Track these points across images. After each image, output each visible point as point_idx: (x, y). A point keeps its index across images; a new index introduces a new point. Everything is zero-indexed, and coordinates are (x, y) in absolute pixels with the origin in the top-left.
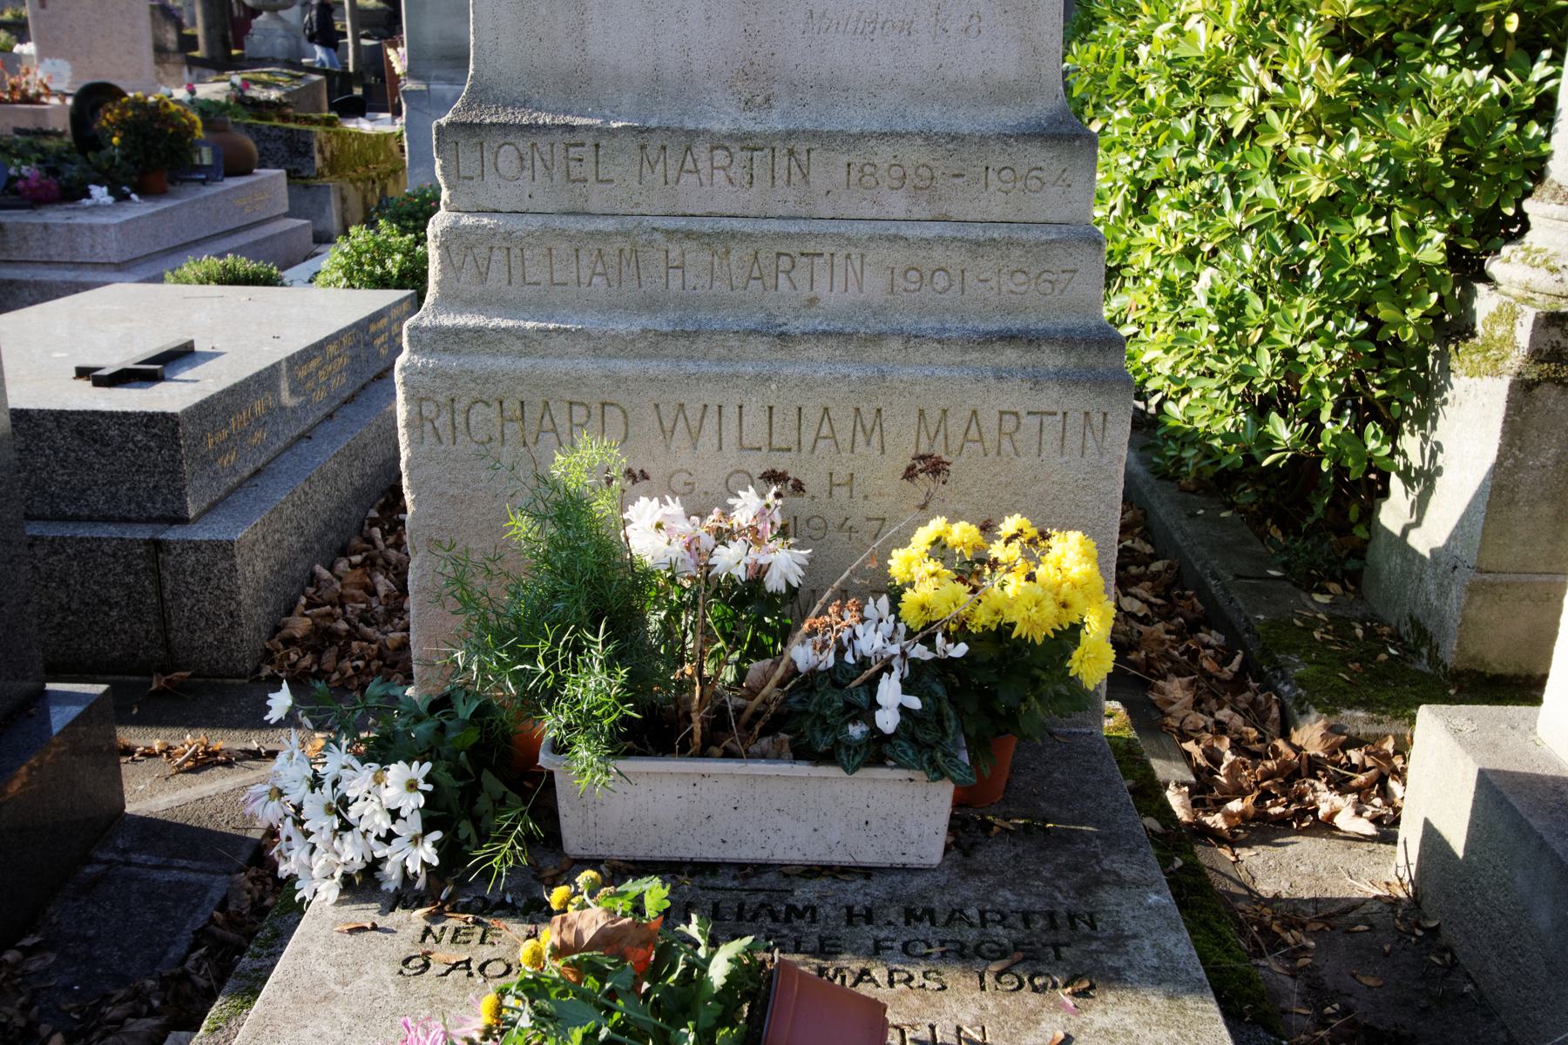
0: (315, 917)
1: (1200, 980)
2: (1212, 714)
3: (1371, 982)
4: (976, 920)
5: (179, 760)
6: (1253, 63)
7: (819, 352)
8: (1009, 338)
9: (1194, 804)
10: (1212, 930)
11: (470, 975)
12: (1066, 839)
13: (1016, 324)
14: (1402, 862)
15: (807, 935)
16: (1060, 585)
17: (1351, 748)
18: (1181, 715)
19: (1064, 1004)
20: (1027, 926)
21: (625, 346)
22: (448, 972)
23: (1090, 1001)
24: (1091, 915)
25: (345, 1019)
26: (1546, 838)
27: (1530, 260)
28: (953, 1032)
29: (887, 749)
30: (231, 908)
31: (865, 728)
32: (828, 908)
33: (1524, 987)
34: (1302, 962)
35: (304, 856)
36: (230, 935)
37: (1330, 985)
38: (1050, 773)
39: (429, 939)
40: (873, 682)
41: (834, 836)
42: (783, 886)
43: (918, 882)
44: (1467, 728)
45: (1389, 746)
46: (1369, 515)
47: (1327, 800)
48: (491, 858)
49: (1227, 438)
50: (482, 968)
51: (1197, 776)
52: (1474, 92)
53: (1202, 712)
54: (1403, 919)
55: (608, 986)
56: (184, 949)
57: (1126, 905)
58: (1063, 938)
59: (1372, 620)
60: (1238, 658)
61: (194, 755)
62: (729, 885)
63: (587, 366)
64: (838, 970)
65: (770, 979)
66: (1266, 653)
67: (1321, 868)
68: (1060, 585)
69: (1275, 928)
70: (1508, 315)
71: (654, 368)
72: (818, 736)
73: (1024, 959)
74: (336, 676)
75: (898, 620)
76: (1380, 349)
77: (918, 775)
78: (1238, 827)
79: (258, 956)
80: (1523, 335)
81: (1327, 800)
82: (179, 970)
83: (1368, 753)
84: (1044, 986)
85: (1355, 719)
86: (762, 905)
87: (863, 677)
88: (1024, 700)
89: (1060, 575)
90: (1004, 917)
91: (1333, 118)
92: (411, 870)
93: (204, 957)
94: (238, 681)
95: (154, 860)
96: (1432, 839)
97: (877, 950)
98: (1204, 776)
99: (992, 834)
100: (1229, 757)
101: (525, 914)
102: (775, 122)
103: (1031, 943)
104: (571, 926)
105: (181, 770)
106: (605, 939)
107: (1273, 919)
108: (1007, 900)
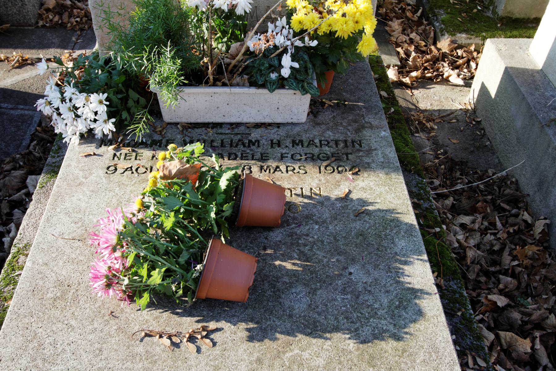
0: (71, 150)
1: (398, 167)
2: (408, 35)
3: (455, 141)
4: (318, 144)
5: (13, 63)
9: (399, 73)
10: (403, 137)
11: (133, 173)
12: (352, 109)
14: (472, 98)
15: (256, 152)
16: (355, 13)
17: (459, 49)
18: (397, 36)
19: (349, 178)
20: (337, 147)
22: (124, 172)
23: (358, 176)
24: (360, 141)
25: (88, 193)
26: (525, 95)
28: (309, 190)
29: (285, 82)
30: (43, 125)
31: (277, 75)
32: (264, 141)
33: (508, 145)
34: (432, 134)
35: (63, 127)
36: (45, 136)
37: (441, 143)
38: (348, 80)
39: (116, 158)
41: (266, 113)
42: (247, 132)
43: (297, 129)
44: (503, 49)
45: (472, 48)
47: (446, 70)
48: (135, 130)
50: (137, 170)
51: (401, 62)
53: (405, 34)
54: (469, 118)
55: (182, 190)
56: (28, 141)
57: (373, 136)
58: (349, 151)
60: (420, 11)
61: (18, 61)
62: (227, 132)
64: (268, 167)
65: (243, 183)
66: (431, 9)
67: (442, 97)
68: (355, 13)
69: (424, 122)
72: (259, 77)
73: (336, 160)
74: (69, 25)
75: (290, 28)
77: (298, 92)
78: (414, 81)
79: (54, 157)
81: (446, 70)
82: (27, 151)
83: (464, 51)
84: (342, 171)
85: (462, 38)
86: (239, 140)
87: (276, 53)
88: (339, 60)
90: (328, 143)
92: (105, 133)
93: (37, 145)
94: (30, 28)
95: (10, 106)
96: (484, 89)
97: (282, 158)
98: (403, 61)
99: (325, 107)
100: (413, 54)
101: (151, 147)
103: (338, 154)
104: (167, 168)
105: (14, 68)
106: (180, 174)
107: (424, 118)
108: (330, 136)
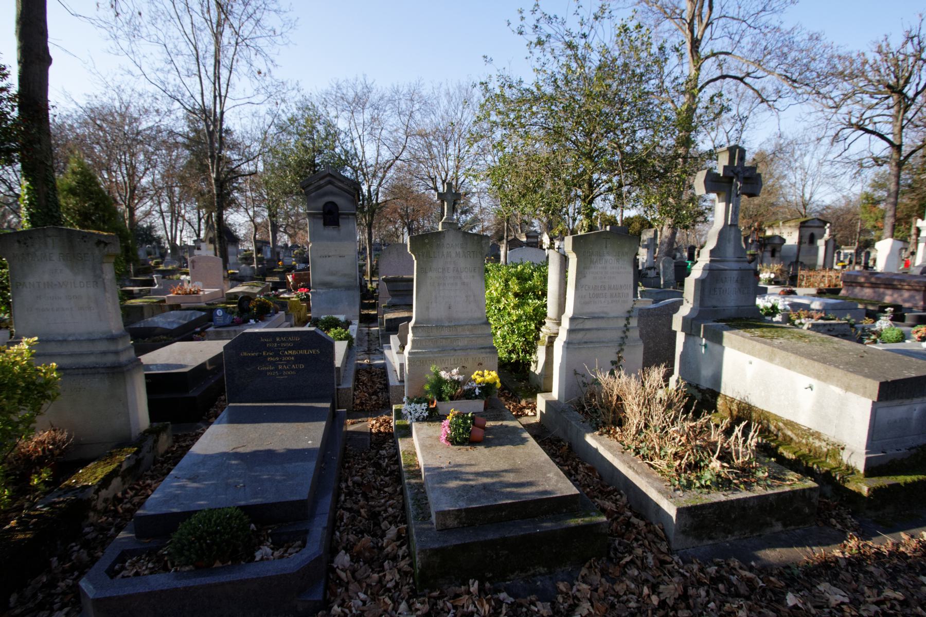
21: (436, 353)
46: (529, 369)
47: (527, 411)
70: (544, 337)
76: (527, 342)
89: (491, 376)
91: (516, 307)
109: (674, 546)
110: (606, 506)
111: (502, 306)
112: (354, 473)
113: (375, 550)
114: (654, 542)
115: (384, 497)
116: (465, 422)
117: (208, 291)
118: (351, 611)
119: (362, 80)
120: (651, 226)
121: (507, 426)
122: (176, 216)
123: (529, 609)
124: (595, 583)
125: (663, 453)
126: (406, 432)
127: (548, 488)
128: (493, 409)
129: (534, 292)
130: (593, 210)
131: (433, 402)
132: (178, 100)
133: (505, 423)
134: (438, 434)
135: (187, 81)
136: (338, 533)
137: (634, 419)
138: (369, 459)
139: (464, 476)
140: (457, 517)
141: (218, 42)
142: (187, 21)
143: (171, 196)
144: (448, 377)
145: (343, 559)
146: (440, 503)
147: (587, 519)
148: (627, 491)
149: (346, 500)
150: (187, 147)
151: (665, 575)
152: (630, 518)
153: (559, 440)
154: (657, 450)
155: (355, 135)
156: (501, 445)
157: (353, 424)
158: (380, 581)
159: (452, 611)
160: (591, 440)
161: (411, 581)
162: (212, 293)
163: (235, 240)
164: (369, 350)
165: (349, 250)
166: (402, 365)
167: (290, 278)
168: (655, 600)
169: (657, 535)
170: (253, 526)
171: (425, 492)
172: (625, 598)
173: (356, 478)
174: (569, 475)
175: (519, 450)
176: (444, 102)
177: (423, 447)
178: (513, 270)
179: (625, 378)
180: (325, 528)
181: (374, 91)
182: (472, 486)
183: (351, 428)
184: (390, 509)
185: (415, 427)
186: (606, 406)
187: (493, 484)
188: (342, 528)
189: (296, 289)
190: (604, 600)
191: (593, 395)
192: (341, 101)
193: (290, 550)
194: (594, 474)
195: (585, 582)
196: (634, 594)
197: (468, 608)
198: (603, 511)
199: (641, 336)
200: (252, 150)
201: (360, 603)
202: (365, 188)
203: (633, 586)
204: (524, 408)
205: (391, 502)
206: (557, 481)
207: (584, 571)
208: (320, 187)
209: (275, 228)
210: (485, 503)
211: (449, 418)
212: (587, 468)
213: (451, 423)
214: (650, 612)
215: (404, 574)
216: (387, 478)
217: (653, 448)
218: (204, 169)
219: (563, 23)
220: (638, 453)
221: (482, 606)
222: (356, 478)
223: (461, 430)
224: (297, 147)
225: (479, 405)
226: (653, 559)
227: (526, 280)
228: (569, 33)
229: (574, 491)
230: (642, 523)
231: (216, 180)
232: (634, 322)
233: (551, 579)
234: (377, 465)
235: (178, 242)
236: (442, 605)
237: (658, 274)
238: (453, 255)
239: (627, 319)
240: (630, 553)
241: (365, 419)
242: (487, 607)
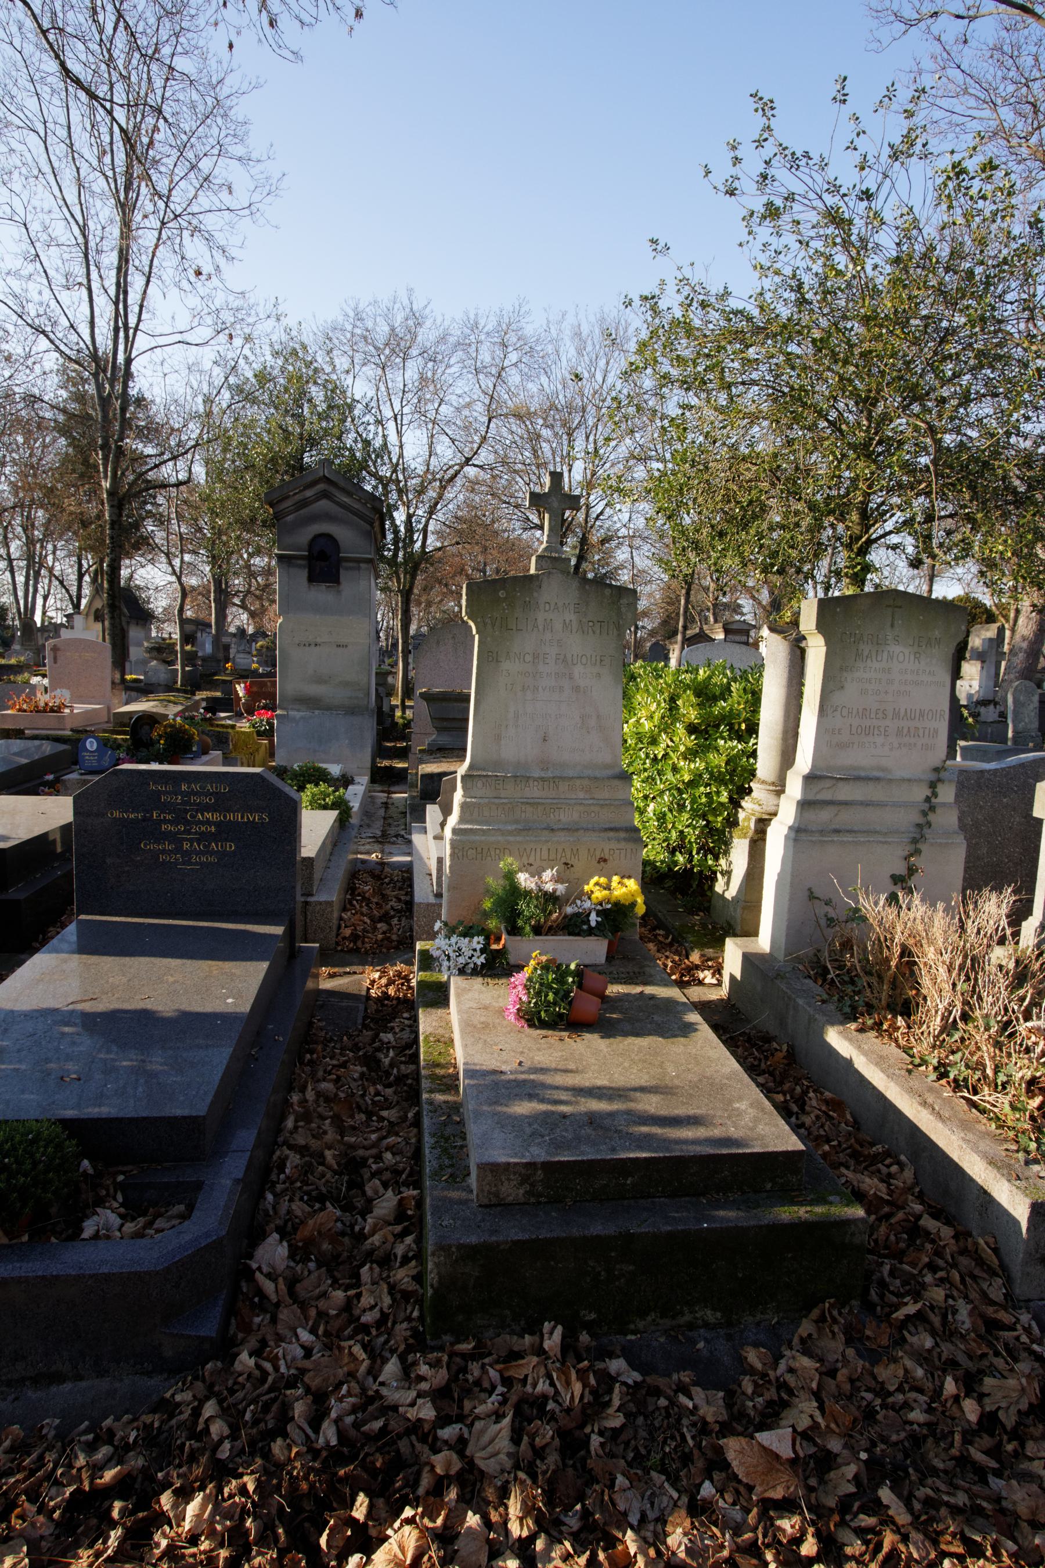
6: (664, 736)
7: (562, 834)
8: (611, 829)
13: (612, 825)
21: (510, 833)
27: (754, 801)
40: (589, 915)
46: (712, 887)
49: (662, 862)
52: (733, 748)
59: (714, 924)
63: (500, 838)
71: (518, 839)
76: (710, 830)
80: (752, 825)
89: (627, 888)
91: (691, 754)
96: (732, 977)
102: (550, 774)
109: (1020, 1290)
110: (864, 1187)
111: (660, 753)
112: (320, 1073)
113: (346, 1240)
114: (974, 1278)
115: (378, 1129)
116: (561, 980)
117: (79, 708)
118: (276, 1368)
119: (406, 302)
120: (991, 618)
121: (652, 997)
122: (35, 566)
123: (673, 1403)
124: (831, 1357)
125: (1002, 1078)
126: (437, 996)
127: (733, 1132)
128: (625, 961)
129: (731, 726)
130: (867, 568)
131: (498, 939)
132: (43, 332)
133: (649, 990)
134: (501, 1003)
135: (64, 296)
136: (270, 1197)
137: (938, 990)
138: (356, 1048)
139: (549, 1094)
140: (524, 1180)
141: (126, 224)
142: (67, 175)
143: (28, 526)
144: (533, 886)
145: (274, 1252)
146: (490, 1146)
147: (819, 1210)
148: (914, 1158)
149: (296, 1128)
150: (63, 430)
151: (997, 1354)
152: (919, 1217)
153: (768, 1039)
154: (989, 1072)
155: (388, 413)
156: (637, 1034)
157: (332, 976)
158: (348, 1306)
159: (500, 1389)
160: (838, 1040)
161: (416, 1314)
162: (87, 712)
163: (144, 616)
164: (384, 834)
165: (354, 633)
166: (440, 861)
167: (240, 690)
168: (971, 1409)
169: (980, 1262)
170: (86, 1163)
171: (461, 1123)
172: (900, 1397)
173: (324, 1085)
174: (784, 1111)
175: (676, 1048)
176: (569, 350)
177: (468, 1026)
178: (687, 677)
179: (922, 909)
180: (237, 1181)
181: (428, 323)
182: (564, 1116)
183: (327, 985)
184: (388, 1156)
185: (456, 984)
186: (876, 970)
187: (611, 1115)
188: (279, 1187)
189: (250, 711)
190: (850, 1398)
191: (847, 945)
192: (362, 345)
193: (159, 1223)
194: (842, 1115)
195: (807, 1352)
196: (921, 1391)
197: (535, 1385)
198: (858, 1196)
199: (962, 827)
200: (184, 437)
201: (299, 1352)
202: (400, 517)
203: (920, 1372)
204: (697, 967)
205: (391, 1140)
206: (756, 1120)
207: (806, 1328)
208: (304, 503)
209: (223, 596)
210: (589, 1154)
211: (527, 971)
212: (827, 1102)
213: (530, 979)
214: (957, 1437)
215: (401, 1296)
216: (389, 1091)
217: (980, 1066)
218: (88, 473)
219: (823, 166)
220: (943, 1075)
221: (568, 1384)
222: (324, 1085)
223: (551, 997)
224: (269, 432)
225: (596, 949)
226: (971, 1314)
227: (715, 699)
228: (834, 188)
229: (793, 1143)
230: (947, 1232)
231: (111, 493)
232: (947, 794)
233: (729, 1337)
234: (371, 1062)
235: (38, 618)
236: (477, 1373)
237: (1003, 715)
238: (558, 626)
239: (933, 785)
240: (917, 1297)
241: (358, 969)
242: (577, 1387)
